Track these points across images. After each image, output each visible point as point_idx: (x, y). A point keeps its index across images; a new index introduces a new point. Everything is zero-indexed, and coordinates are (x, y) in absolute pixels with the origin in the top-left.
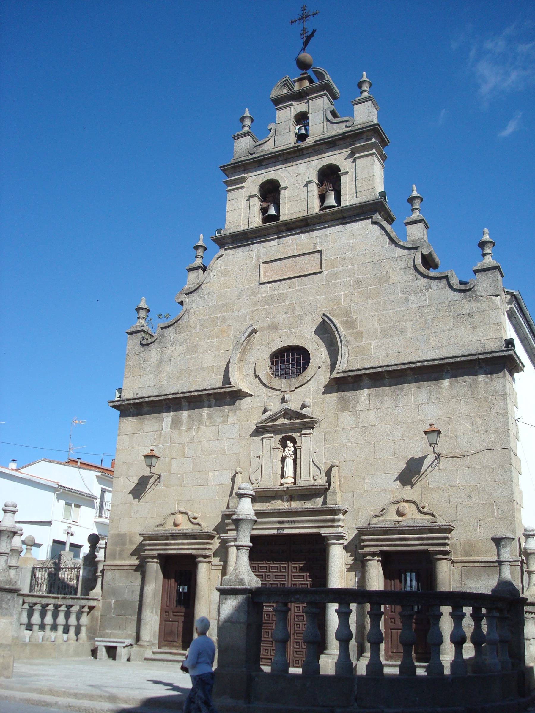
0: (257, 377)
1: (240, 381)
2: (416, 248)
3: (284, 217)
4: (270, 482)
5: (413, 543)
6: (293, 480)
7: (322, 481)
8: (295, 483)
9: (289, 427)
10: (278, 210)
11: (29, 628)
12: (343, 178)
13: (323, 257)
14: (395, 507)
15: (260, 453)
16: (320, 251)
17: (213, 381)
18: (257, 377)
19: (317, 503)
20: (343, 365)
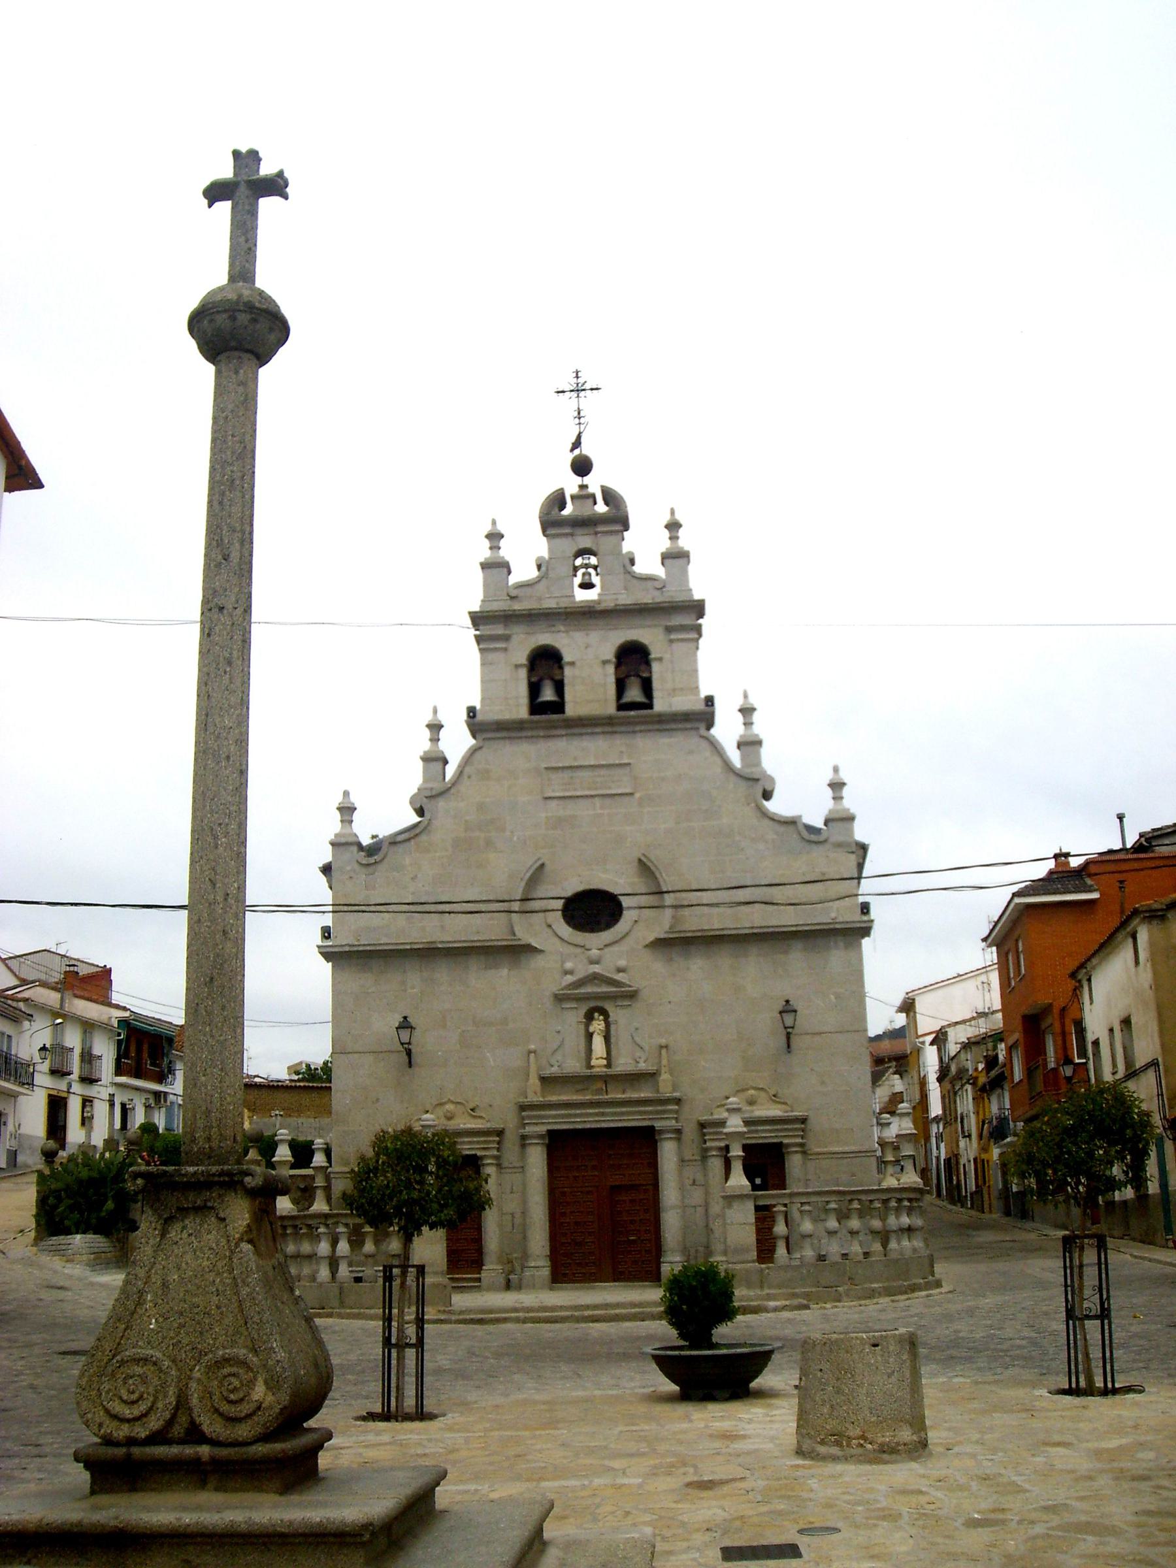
3: (571, 710)
4: (573, 1065)
5: (766, 1136)
8: (609, 1066)
10: (559, 687)
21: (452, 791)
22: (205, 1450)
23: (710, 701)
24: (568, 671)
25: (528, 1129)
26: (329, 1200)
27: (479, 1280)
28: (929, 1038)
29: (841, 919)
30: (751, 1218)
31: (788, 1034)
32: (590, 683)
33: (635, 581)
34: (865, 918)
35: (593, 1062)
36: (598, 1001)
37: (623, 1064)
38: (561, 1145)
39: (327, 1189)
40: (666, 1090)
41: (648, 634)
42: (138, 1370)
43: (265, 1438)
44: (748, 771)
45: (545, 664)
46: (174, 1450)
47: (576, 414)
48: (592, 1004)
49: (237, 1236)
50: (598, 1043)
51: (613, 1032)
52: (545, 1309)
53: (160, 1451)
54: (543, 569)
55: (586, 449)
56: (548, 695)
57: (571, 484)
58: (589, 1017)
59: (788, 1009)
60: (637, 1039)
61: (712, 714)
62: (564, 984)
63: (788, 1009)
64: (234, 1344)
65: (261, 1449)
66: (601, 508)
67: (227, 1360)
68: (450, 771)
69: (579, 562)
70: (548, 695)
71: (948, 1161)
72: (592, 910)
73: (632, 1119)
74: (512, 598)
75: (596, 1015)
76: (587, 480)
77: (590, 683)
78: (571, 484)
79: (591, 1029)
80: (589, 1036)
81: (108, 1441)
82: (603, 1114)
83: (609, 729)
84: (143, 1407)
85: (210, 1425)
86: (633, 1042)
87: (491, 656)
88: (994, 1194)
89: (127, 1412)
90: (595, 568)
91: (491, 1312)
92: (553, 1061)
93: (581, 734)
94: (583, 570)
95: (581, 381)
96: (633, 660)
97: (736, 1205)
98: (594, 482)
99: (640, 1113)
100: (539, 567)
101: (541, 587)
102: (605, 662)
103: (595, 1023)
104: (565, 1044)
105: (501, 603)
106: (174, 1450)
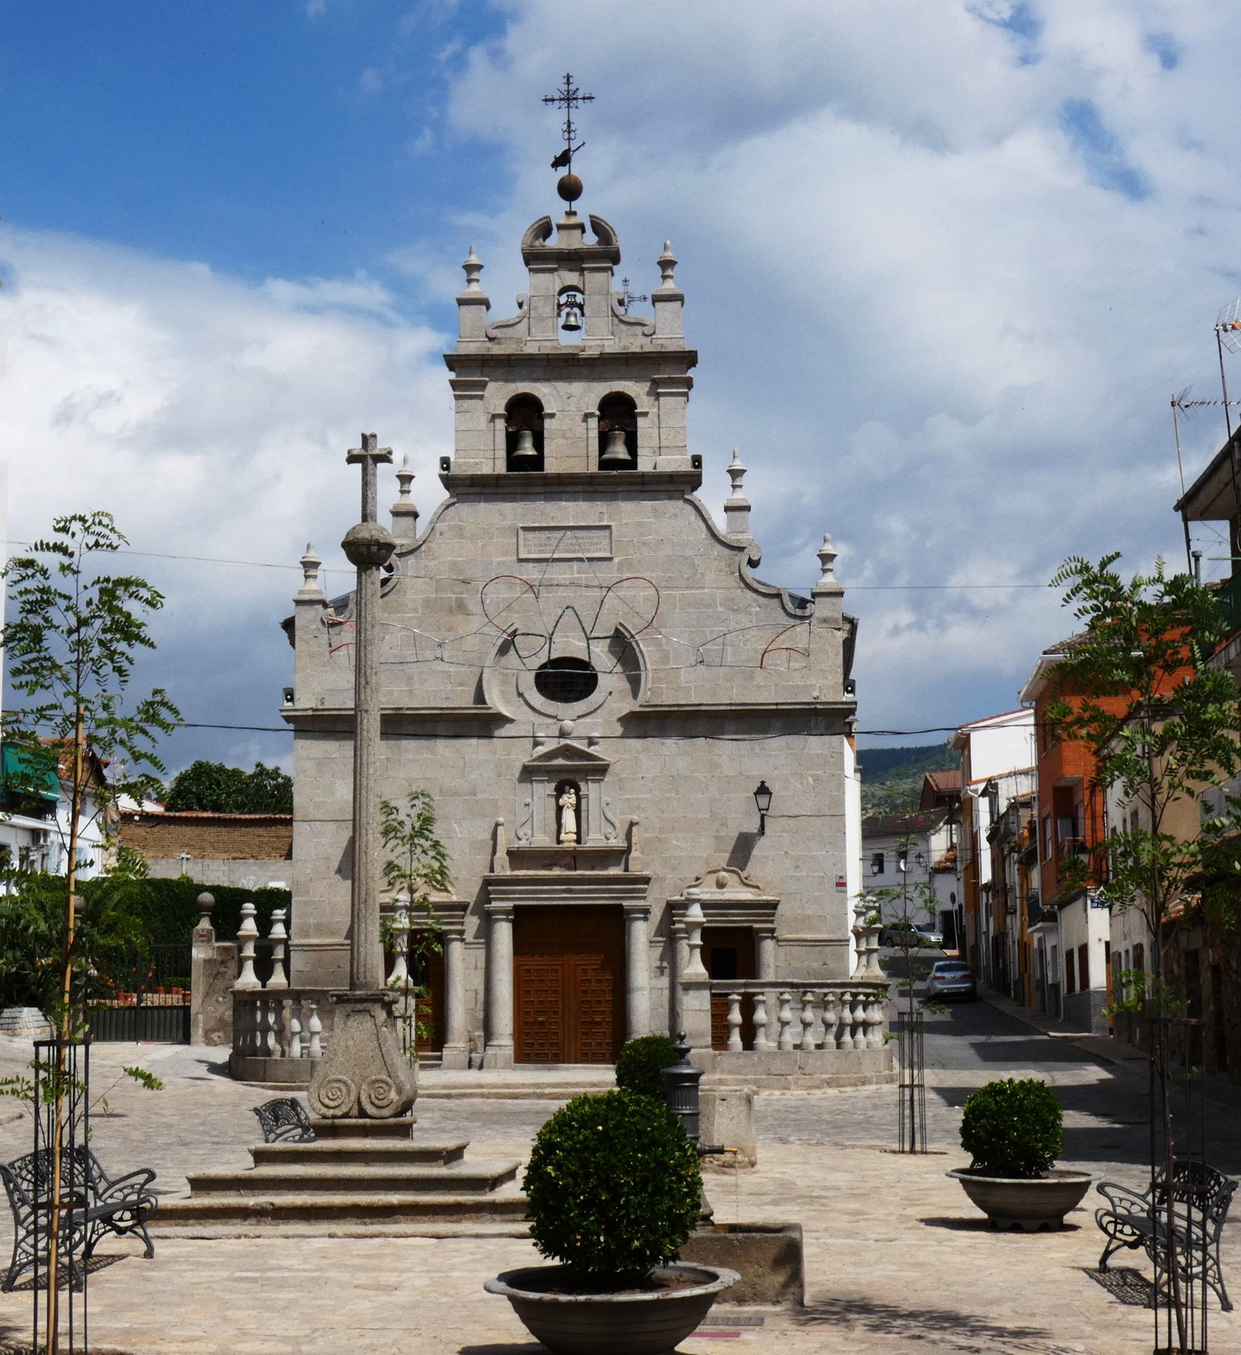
0: (521, 695)
1: (497, 702)
2: (741, 549)
3: (552, 466)
4: (543, 840)
5: (737, 919)
6: (574, 837)
7: (617, 842)
8: (578, 841)
9: (569, 772)
10: (539, 443)
11: (722, 1000)
12: (641, 422)
13: (614, 536)
14: (713, 877)
15: (528, 800)
16: (608, 527)
17: (463, 700)
18: (521, 695)
19: (614, 871)
20: (645, 695)
21: (423, 548)
22: (368, 1121)
23: (697, 461)
24: (548, 423)
25: (494, 904)
26: (288, 975)
27: (440, 1058)
28: (981, 787)
29: (823, 699)
30: (708, 1006)
31: (763, 817)
32: (570, 441)
33: (623, 326)
34: (848, 697)
35: (563, 836)
36: (569, 772)
37: (595, 840)
38: (522, 918)
39: (286, 963)
40: (636, 869)
41: (636, 389)
42: (336, 1085)
43: (395, 1116)
44: (732, 539)
45: (525, 416)
46: (354, 1121)
47: (565, 127)
48: (563, 777)
49: (149, 1004)
50: (569, 818)
51: (584, 807)
52: (508, 1086)
53: (347, 1121)
54: (525, 307)
55: (577, 168)
56: (527, 449)
57: (557, 209)
58: (560, 792)
59: (763, 790)
60: (610, 816)
61: (700, 476)
62: (535, 755)
63: (763, 790)
64: (379, 1073)
65: (392, 1120)
66: (590, 240)
67: (377, 1081)
68: (422, 525)
69: (563, 299)
70: (527, 449)
71: (995, 938)
72: (566, 680)
73: (601, 899)
74: (491, 339)
75: (567, 788)
76: (576, 205)
77: (570, 441)
78: (557, 209)
79: (561, 802)
80: (560, 810)
81: (324, 1117)
82: (570, 891)
83: (587, 488)
84: (339, 1102)
85: (370, 1110)
86: (603, 816)
87: (466, 404)
88: (1033, 985)
89: (332, 1104)
90: (581, 307)
91: (455, 1087)
92: (521, 834)
93: (562, 493)
94: (568, 310)
95: (572, 87)
96: (618, 416)
97: (691, 993)
98: (584, 208)
99: (608, 891)
100: (520, 305)
101: (523, 326)
102: (587, 416)
103: (565, 797)
104: (534, 819)
105: (478, 345)
106: (354, 1121)
